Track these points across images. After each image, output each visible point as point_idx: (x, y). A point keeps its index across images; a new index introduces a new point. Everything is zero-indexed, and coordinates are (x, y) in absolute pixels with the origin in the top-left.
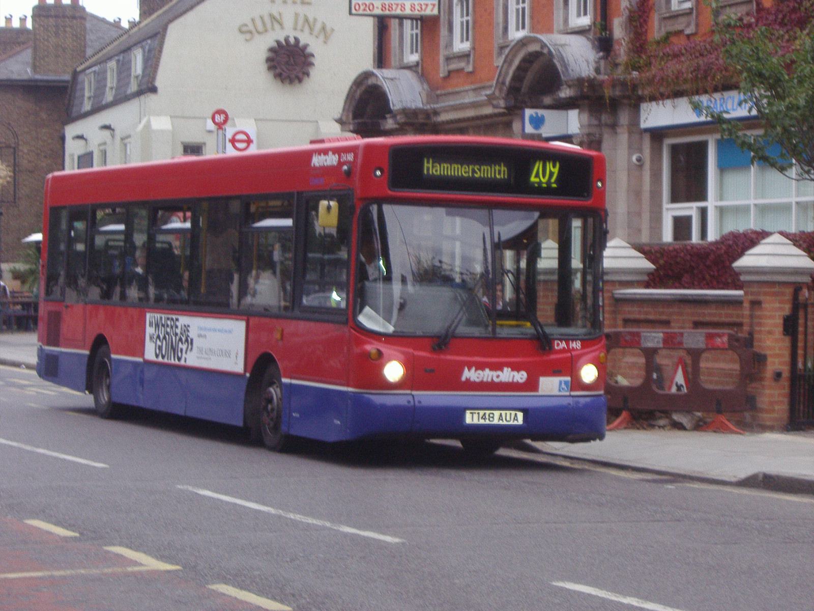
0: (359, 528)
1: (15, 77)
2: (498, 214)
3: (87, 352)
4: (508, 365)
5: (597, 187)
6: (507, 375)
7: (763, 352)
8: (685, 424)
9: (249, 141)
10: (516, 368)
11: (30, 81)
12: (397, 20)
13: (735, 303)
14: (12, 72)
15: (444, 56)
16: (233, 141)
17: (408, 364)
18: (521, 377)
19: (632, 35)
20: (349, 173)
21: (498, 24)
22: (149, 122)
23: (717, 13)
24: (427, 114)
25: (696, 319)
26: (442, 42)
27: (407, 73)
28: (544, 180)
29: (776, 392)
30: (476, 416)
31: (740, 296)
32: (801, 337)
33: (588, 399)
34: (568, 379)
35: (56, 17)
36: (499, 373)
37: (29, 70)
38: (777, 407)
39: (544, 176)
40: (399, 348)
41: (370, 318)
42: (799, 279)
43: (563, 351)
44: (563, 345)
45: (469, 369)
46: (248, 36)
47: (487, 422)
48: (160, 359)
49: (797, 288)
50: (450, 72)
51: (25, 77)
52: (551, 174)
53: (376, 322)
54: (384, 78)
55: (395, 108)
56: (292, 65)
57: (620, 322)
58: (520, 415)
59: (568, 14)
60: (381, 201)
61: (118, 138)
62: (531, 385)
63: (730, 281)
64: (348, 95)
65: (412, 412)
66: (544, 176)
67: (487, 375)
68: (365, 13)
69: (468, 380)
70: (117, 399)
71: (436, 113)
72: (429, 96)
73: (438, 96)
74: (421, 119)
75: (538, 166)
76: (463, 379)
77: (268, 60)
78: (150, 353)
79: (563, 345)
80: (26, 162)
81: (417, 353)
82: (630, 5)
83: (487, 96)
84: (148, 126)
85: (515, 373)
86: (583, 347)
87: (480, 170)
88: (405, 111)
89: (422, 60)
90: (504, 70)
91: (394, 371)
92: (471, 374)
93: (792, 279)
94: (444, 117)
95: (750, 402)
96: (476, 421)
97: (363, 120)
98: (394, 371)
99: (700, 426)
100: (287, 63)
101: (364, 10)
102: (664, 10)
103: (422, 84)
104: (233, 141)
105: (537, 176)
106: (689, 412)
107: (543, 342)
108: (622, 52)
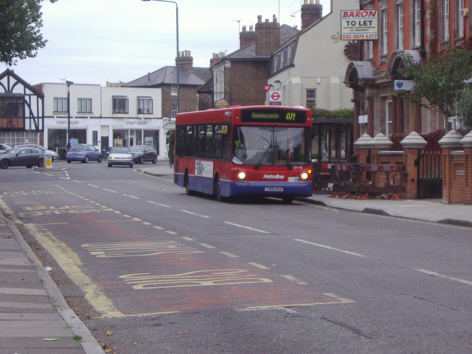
0: (244, 226)
1: (247, 57)
2: (276, 129)
3: (184, 174)
4: (278, 174)
5: (308, 120)
6: (278, 177)
7: (407, 172)
8: (385, 197)
9: (279, 96)
10: (281, 174)
11: (254, 58)
12: (367, 41)
13: (401, 155)
14: (246, 55)
15: (380, 56)
16: (272, 96)
17: (247, 174)
18: (282, 177)
19: (431, 51)
20: (231, 117)
21: (395, 44)
22: (291, 80)
23: (455, 44)
24: (373, 80)
25: (396, 161)
26: (379, 50)
27: (368, 63)
28: (290, 118)
29: (412, 186)
30: (268, 188)
31: (403, 153)
32: (421, 167)
33: (307, 184)
34: (298, 178)
35: (266, 28)
36: (275, 176)
37: (254, 53)
38: (412, 191)
39: (291, 117)
40: (245, 169)
41: (236, 160)
42: (420, 147)
43: (296, 169)
44: (296, 167)
45: (266, 175)
46: (336, 40)
47: (272, 190)
48: (198, 175)
49: (420, 150)
50: (382, 63)
51: (252, 57)
52: (293, 116)
53: (238, 161)
54: (357, 65)
55: (360, 78)
56: (356, 52)
57: (380, 163)
58: (282, 189)
59: (415, 41)
60: (240, 126)
61: (282, 86)
62: (286, 179)
63: (436, 148)
64: (346, 73)
65: (249, 188)
66: (291, 117)
67: (271, 177)
68: (347, 39)
69: (265, 178)
70: (190, 189)
71: (376, 80)
72: (374, 72)
73: (379, 72)
74: (370, 82)
75: (289, 114)
76: (264, 178)
77: (345, 51)
78: (196, 174)
79: (296, 167)
80: (253, 96)
81: (250, 170)
82: (431, 39)
83: (385, 74)
84: (290, 81)
85: (281, 176)
86: (303, 168)
87: (270, 116)
88: (364, 79)
89: (374, 57)
90: (390, 64)
91: (242, 175)
92: (266, 176)
93: (418, 147)
94: (378, 82)
95: (404, 189)
96: (268, 190)
97: (353, 82)
98: (242, 175)
99: (390, 198)
100: (354, 52)
101: (347, 38)
102: (442, 41)
103: (373, 67)
104: (272, 96)
105: (288, 117)
106: (386, 193)
107: (290, 167)
108: (429, 56)
